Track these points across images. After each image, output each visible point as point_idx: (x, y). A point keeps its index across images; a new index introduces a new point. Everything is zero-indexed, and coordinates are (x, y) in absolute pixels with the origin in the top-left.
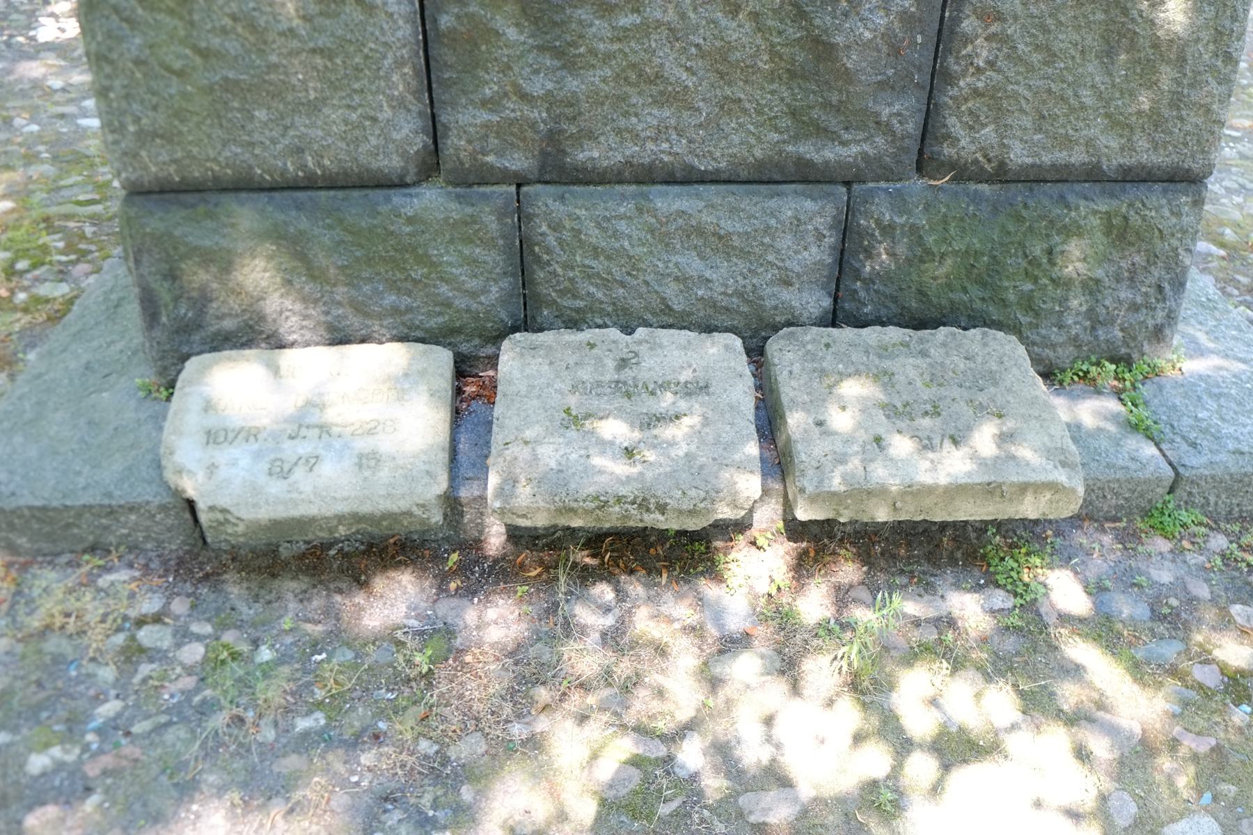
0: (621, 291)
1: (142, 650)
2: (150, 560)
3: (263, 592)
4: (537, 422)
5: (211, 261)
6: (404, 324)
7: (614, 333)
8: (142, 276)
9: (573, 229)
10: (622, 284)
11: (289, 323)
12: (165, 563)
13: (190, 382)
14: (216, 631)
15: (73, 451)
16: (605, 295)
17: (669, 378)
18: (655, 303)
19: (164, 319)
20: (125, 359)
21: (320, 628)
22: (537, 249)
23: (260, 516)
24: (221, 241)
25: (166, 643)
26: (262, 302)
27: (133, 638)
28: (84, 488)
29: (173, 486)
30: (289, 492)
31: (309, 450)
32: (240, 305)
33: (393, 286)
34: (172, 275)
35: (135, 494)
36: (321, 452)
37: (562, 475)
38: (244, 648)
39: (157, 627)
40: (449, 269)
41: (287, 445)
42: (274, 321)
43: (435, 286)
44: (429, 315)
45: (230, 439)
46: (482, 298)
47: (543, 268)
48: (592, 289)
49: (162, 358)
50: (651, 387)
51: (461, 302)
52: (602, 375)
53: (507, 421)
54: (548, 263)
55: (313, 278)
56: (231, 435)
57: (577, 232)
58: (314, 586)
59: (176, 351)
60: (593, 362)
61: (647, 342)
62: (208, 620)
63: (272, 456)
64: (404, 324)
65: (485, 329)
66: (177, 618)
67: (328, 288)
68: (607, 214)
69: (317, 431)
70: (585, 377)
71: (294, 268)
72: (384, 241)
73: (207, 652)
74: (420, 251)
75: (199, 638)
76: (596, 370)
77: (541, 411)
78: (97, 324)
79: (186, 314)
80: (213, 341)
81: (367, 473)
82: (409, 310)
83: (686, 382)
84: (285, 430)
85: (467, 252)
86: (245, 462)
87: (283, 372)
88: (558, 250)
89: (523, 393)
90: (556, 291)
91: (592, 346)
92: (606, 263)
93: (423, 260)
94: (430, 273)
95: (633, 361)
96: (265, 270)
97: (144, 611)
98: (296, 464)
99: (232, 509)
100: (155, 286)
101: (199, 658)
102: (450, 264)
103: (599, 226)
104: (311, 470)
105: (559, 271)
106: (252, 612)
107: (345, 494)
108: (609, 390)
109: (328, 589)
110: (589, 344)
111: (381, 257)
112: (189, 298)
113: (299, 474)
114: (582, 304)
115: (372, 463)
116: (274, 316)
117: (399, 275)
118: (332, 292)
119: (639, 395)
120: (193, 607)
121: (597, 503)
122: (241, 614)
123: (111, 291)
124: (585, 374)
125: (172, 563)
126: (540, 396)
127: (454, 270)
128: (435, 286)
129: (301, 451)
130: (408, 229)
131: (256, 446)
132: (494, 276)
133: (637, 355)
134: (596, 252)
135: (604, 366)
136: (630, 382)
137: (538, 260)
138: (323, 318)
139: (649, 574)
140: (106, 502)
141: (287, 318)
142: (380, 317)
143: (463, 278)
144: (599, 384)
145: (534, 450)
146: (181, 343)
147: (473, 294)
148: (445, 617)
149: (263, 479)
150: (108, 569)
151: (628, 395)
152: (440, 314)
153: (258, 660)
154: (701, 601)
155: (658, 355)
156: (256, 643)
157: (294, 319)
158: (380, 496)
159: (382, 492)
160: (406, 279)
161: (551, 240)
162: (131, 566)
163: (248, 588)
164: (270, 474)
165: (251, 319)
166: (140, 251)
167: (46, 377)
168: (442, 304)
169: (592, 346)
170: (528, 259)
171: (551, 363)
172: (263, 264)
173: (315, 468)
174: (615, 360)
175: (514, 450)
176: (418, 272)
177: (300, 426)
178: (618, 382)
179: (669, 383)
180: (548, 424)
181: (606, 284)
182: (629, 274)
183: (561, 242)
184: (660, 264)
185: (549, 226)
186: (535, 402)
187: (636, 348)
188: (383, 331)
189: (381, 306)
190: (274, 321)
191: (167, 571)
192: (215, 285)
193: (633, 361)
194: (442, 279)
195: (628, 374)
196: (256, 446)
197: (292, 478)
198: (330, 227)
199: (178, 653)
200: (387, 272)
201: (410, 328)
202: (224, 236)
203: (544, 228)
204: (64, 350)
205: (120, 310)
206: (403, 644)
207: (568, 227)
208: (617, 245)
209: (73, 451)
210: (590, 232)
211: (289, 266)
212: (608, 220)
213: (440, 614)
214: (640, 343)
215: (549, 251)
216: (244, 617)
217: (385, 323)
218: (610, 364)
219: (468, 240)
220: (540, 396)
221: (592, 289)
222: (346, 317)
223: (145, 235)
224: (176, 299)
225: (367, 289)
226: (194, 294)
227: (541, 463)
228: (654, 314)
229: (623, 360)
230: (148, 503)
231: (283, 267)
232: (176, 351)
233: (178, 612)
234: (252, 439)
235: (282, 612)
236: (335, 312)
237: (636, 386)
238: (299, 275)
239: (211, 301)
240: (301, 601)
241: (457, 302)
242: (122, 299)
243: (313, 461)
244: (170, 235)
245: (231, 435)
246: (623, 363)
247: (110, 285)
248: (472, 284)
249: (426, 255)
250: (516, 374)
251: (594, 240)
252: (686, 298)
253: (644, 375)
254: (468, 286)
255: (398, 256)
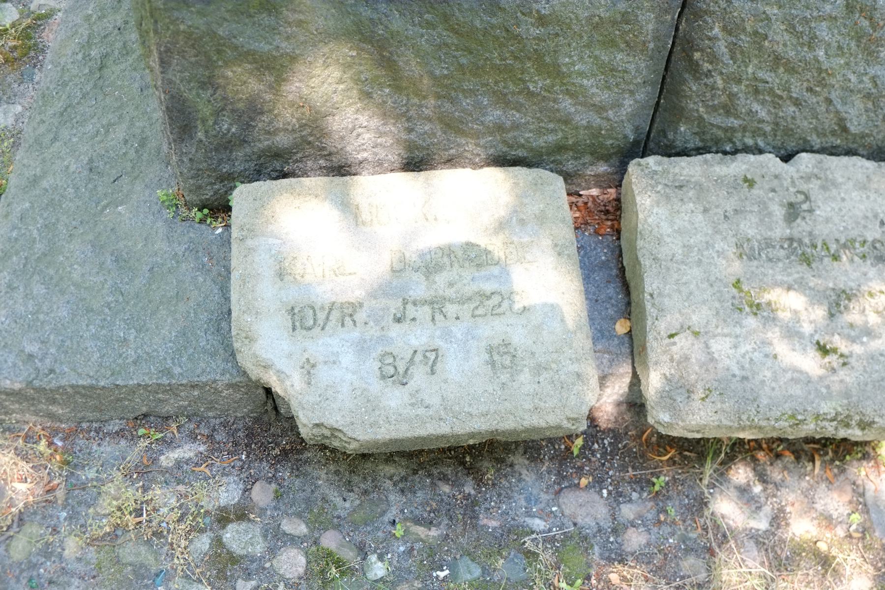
0: (792, 109)
1: (233, 559)
2: (214, 430)
3: (356, 479)
4: (704, 302)
5: (268, 68)
6: (505, 142)
7: (771, 160)
8: (170, 82)
9: (756, 33)
10: (797, 103)
11: (360, 141)
12: (232, 434)
13: (252, 232)
14: (311, 531)
15: (108, 306)
16: (769, 112)
17: (854, 234)
18: (829, 122)
19: (200, 135)
20: (132, 154)
21: (434, 532)
22: (697, 55)
23: (379, 437)
24: (284, 45)
25: (259, 548)
26: (330, 118)
27: (218, 542)
28: (135, 363)
29: (254, 378)
30: (412, 405)
31: (424, 340)
32: (298, 120)
33: (502, 100)
34: (208, 83)
35: (199, 371)
36: (439, 343)
37: (748, 385)
38: (349, 555)
39: (244, 525)
40: (578, 80)
41: (395, 331)
42: (342, 138)
43: (555, 101)
44: (539, 132)
45: (321, 322)
46: (611, 113)
47: (697, 79)
48: (756, 107)
49: (195, 177)
50: (833, 247)
51: (583, 117)
52: (771, 229)
53: (666, 301)
54: (709, 74)
55: (397, 88)
56: (321, 316)
57: (759, 37)
58: (415, 472)
59: (215, 170)
60: (756, 208)
61: (817, 177)
62: (299, 515)
63: (380, 350)
64: (505, 142)
65: (602, 146)
66: (263, 511)
67: (416, 101)
68: (807, 14)
69: (427, 309)
70: (751, 232)
71: (377, 77)
72: (501, 45)
73: (308, 562)
74: (548, 59)
75: (293, 540)
76: (761, 221)
77: (705, 285)
78: (84, 96)
79: (229, 130)
80: (260, 157)
81: (504, 377)
82: (516, 126)
83: (874, 241)
84: (386, 309)
85: (605, 58)
86: (348, 359)
87: (365, 216)
88: (726, 58)
89: (679, 257)
90: (707, 107)
91: (750, 183)
92: (786, 77)
93: (555, 72)
94: (553, 86)
95: (805, 207)
96: (340, 81)
97: (223, 502)
98: (411, 361)
99: (345, 430)
100: (190, 96)
101: (301, 570)
102: (581, 74)
103: (791, 29)
104: (433, 372)
105: (720, 83)
106: (347, 505)
107: (483, 408)
108: (782, 253)
109: (430, 475)
110: (746, 180)
111: (494, 67)
112: (233, 111)
113: (419, 377)
114: (735, 123)
115: (507, 360)
116: (343, 133)
117: (512, 87)
118: (421, 106)
119: (821, 260)
120: (278, 497)
121: (792, 422)
122: (335, 507)
123: (89, 44)
124: (749, 227)
125: (240, 434)
126: (700, 261)
127: (585, 82)
128: (555, 101)
129: (415, 342)
130: (536, 31)
131: (356, 334)
132: (632, 87)
133: (807, 198)
134: (777, 60)
135: (770, 214)
136: (807, 241)
137: (694, 68)
138: (404, 136)
139: (798, 458)
140: (165, 381)
141: (359, 135)
142: (477, 135)
143: (594, 90)
144: (768, 244)
145: (707, 346)
146: (220, 161)
147: (600, 109)
148: (574, 516)
149: (376, 386)
150: (169, 444)
151: (807, 260)
152: (553, 131)
153: (371, 576)
154: (859, 492)
155: (834, 199)
156: (362, 551)
157: (367, 136)
158: (525, 411)
159: (527, 406)
160: (520, 93)
161: (722, 47)
162: (193, 437)
163: (337, 473)
164: (383, 377)
165: (311, 135)
166: (168, 50)
167: (45, 184)
168: (559, 121)
169: (750, 183)
170: (679, 63)
171: (706, 211)
172: (337, 74)
173: (439, 367)
174: (782, 205)
175: (683, 343)
176: (537, 84)
177: (405, 302)
178: (791, 240)
179: (853, 241)
180: (717, 305)
181: (776, 101)
182: (810, 90)
183: (733, 48)
184: (853, 78)
185: (724, 29)
186: (696, 272)
187: (804, 187)
188: (478, 150)
189: (482, 123)
190: (342, 138)
191: (236, 444)
192: (268, 97)
193: (805, 207)
194: (568, 92)
195: (801, 227)
196: (356, 334)
197: (412, 384)
198: (430, 25)
199: (275, 562)
200: (496, 83)
201: (511, 147)
202: (288, 38)
203: (716, 30)
204: (55, 139)
205: (106, 72)
206: (535, 555)
207: (749, 29)
208: (810, 56)
209: (108, 306)
210: (778, 38)
211: (368, 75)
212: (806, 21)
213: (567, 512)
214: (807, 178)
215: (714, 59)
216: (343, 514)
217: (482, 142)
218: (779, 212)
219: (610, 43)
220: (700, 261)
221: (756, 107)
222: (434, 134)
223: (177, 33)
224: (217, 113)
225: (467, 103)
226: (240, 106)
227: (720, 366)
228: (821, 134)
229: (791, 205)
230: (215, 381)
231: (363, 78)
232: (215, 170)
233: (262, 504)
234: (348, 321)
235: (384, 506)
236: (419, 129)
237: (814, 246)
238: (381, 86)
239: (262, 113)
240: (402, 491)
241: (577, 118)
242: (106, 56)
243: (432, 356)
244: (213, 35)
245: (321, 316)
246: (793, 212)
247: (84, 31)
248: (602, 96)
249: (557, 66)
250: (666, 228)
251: (780, 49)
252: (869, 119)
253: (822, 231)
254: (596, 100)
255: (518, 65)
